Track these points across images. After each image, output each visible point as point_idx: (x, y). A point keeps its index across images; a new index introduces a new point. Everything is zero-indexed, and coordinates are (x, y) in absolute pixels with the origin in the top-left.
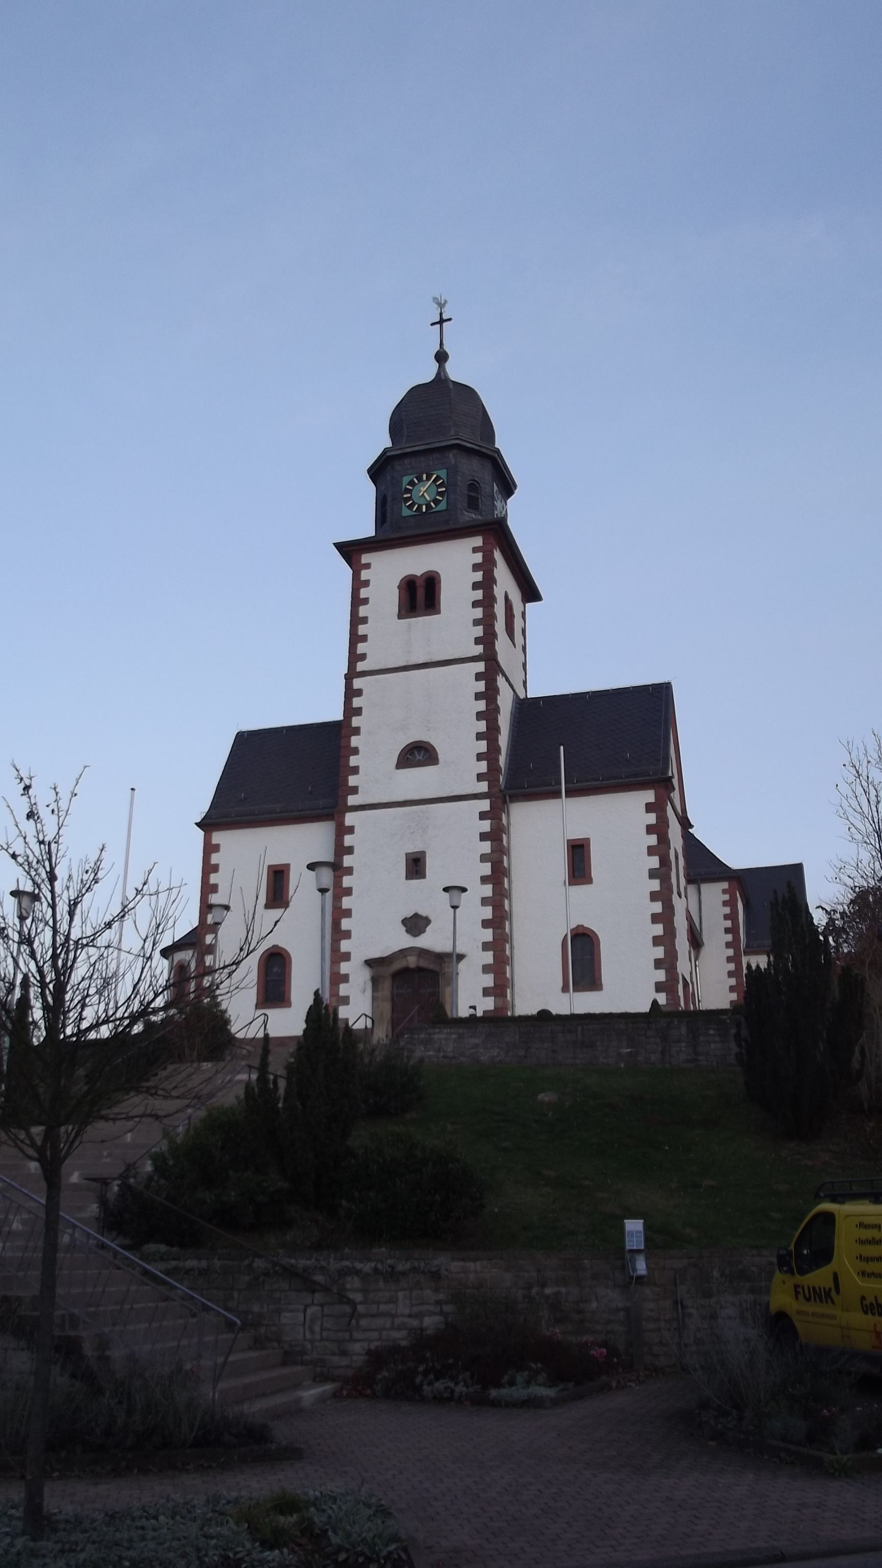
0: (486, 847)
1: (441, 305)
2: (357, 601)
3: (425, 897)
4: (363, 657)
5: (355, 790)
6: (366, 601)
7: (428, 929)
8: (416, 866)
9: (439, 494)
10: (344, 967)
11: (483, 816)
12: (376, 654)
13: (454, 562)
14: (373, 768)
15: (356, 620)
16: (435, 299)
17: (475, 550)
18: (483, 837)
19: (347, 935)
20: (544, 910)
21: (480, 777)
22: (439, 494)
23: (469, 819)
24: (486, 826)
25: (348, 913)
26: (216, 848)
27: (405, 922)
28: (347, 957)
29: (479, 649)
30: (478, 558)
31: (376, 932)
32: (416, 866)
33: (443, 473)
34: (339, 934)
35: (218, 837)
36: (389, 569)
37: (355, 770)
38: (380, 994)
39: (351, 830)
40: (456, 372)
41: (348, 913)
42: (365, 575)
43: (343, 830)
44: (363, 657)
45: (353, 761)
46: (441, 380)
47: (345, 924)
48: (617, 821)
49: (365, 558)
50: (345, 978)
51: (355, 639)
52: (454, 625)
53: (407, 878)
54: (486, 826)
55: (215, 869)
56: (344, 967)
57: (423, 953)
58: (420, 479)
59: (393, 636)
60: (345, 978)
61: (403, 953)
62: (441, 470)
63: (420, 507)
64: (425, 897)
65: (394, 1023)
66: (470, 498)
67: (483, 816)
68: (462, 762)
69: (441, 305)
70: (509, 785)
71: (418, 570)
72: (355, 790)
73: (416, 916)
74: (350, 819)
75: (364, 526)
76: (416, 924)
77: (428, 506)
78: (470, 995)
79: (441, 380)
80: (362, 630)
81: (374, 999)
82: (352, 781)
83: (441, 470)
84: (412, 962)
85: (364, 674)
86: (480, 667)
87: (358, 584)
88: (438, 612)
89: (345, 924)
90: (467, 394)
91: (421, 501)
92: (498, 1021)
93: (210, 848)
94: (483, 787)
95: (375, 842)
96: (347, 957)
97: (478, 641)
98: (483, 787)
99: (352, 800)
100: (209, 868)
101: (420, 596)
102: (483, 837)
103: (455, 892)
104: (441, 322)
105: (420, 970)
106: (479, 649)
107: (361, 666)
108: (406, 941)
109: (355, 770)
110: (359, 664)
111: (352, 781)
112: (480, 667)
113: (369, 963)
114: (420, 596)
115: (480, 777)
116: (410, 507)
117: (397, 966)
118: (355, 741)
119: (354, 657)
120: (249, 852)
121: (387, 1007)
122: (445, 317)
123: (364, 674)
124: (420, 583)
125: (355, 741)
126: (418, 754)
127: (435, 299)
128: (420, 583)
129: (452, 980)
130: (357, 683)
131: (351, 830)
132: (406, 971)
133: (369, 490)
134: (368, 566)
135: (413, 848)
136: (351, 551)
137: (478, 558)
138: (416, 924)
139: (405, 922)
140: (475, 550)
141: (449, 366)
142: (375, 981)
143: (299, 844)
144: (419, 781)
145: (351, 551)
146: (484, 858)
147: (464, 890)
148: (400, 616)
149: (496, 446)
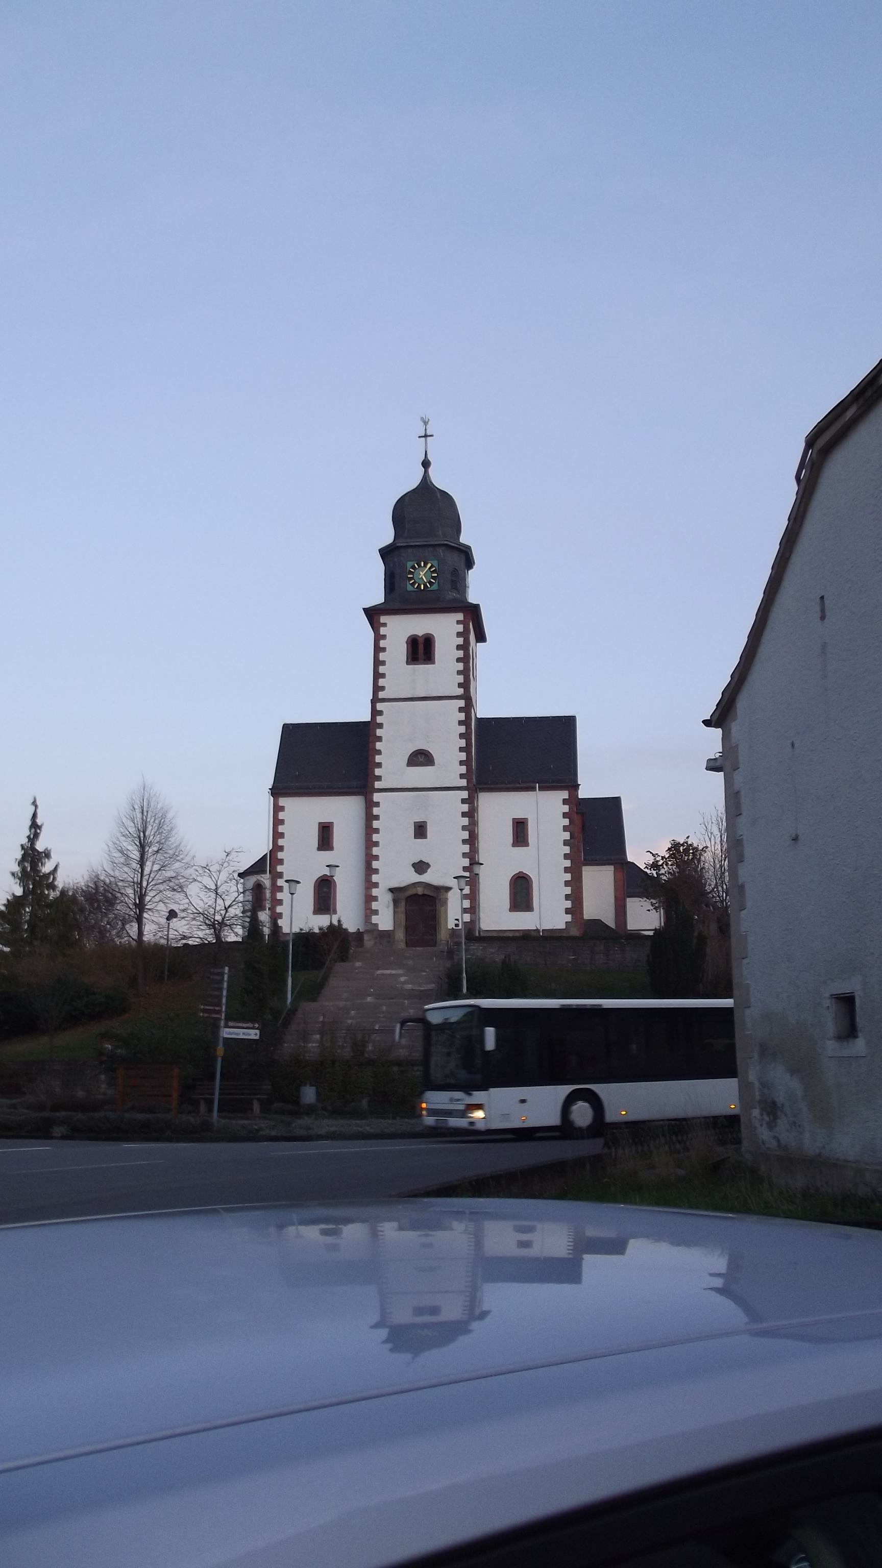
0: (466, 821)
1: (426, 423)
2: (378, 649)
3: (420, 850)
4: (383, 688)
5: (379, 778)
6: (384, 650)
7: (429, 870)
8: (420, 830)
9: (433, 578)
10: (375, 892)
11: (464, 801)
12: (391, 688)
13: (444, 628)
14: (390, 765)
15: (377, 663)
16: (422, 418)
17: (458, 622)
18: (464, 814)
19: (376, 871)
20: (500, 863)
21: (462, 776)
22: (433, 578)
23: (455, 802)
24: (465, 808)
25: (376, 858)
26: (282, 809)
27: (414, 865)
28: (376, 885)
29: (461, 691)
30: (460, 628)
31: (395, 872)
32: (420, 830)
33: (435, 563)
34: (370, 870)
35: (282, 801)
36: (401, 629)
37: (379, 765)
38: (399, 910)
39: (377, 804)
40: (439, 480)
41: (376, 858)
42: (383, 631)
43: (370, 805)
44: (383, 688)
45: (378, 759)
46: (426, 486)
47: (375, 865)
48: (546, 810)
49: (383, 619)
50: (375, 899)
51: (377, 675)
52: (442, 673)
53: (415, 838)
54: (465, 808)
55: (282, 822)
56: (375, 892)
57: (427, 885)
58: (419, 565)
59: (402, 676)
60: (375, 899)
61: (415, 885)
62: (426, 556)
63: (419, 585)
64: (420, 850)
65: (407, 928)
66: (452, 581)
67: (464, 801)
68: (450, 764)
69: (426, 423)
70: (479, 782)
71: (420, 632)
72: (379, 778)
73: (421, 861)
74: (376, 797)
75: (377, 597)
76: (421, 867)
77: (425, 586)
78: (454, 913)
79: (426, 486)
80: (382, 669)
81: (395, 912)
82: (377, 772)
83: (426, 556)
84: (420, 891)
85: (384, 700)
86: (462, 703)
87: (378, 637)
88: (434, 663)
89: (375, 865)
90: (447, 499)
91: (420, 582)
92: (471, 933)
93: (277, 809)
94: (464, 783)
95: (394, 813)
96: (376, 885)
97: (460, 685)
98: (464, 783)
99: (377, 785)
100: (277, 822)
101: (421, 650)
102: (464, 814)
103: (293, 883)
104: (426, 436)
105: (424, 895)
106: (461, 691)
107: (381, 695)
108: (415, 878)
109: (379, 765)
110: (380, 693)
111: (377, 772)
112: (462, 703)
113: (391, 890)
114: (421, 650)
115: (462, 776)
116: (413, 584)
117: (410, 892)
118: (378, 745)
119: (377, 688)
120: (306, 813)
121: (403, 917)
122: (428, 433)
123: (384, 700)
124: (421, 641)
125: (378, 745)
126: (421, 758)
127: (422, 418)
128: (421, 641)
129: (445, 902)
130: (379, 706)
131: (377, 804)
132: (416, 895)
133: (378, 569)
134: (385, 625)
135: (418, 819)
136: (372, 614)
137: (460, 628)
138: (421, 867)
139: (414, 865)
140: (458, 622)
141: (431, 471)
142: (396, 902)
143: (342, 811)
144: (421, 775)
145: (372, 614)
146: (464, 828)
147: (298, 882)
148: (408, 663)
149: (464, 539)
